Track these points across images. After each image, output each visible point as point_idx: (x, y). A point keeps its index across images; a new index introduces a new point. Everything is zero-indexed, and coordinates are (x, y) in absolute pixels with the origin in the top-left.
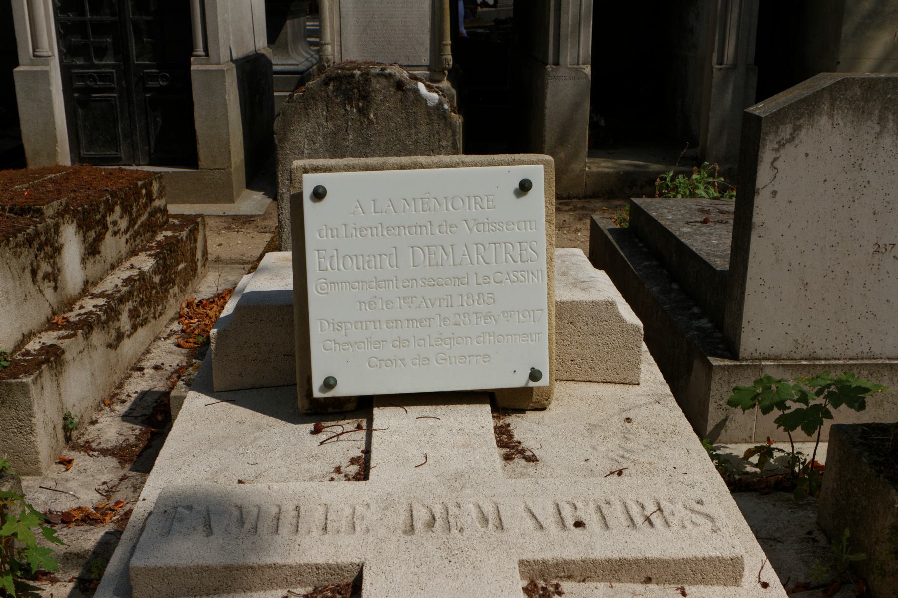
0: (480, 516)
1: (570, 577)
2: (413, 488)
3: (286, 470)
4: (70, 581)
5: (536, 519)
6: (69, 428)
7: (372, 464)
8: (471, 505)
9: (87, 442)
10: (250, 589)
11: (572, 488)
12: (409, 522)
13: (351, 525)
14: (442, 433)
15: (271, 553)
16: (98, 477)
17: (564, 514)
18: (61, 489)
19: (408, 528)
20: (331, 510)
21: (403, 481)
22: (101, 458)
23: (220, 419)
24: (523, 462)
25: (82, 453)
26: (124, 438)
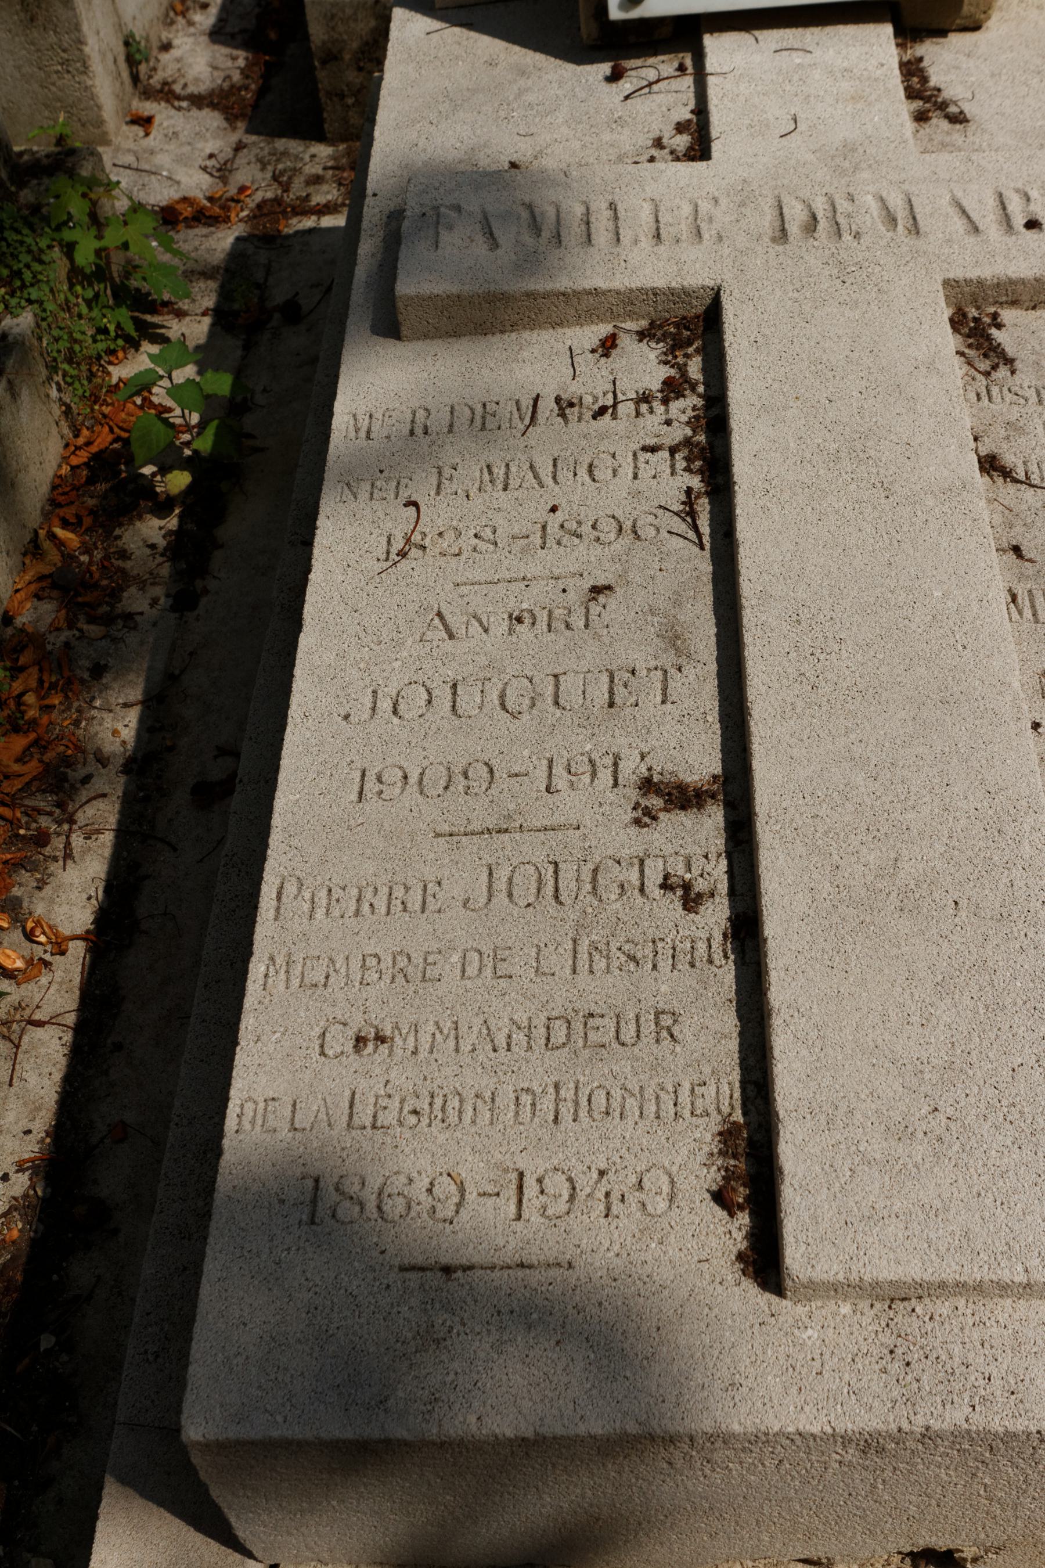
0: (884, 213)
1: (1014, 303)
2: (781, 171)
3: (577, 145)
4: (204, 314)
5: (968, 217)
6: (134, 56)
7: (714, 133)
8: (870, 197)
9: (165, 83)
10: (561, 324)
11: (1024, 168)
12: (778, 223)
13: (694, 231)
14: (817, 77)
15: (588, 273)
16: (200, 145)
17: (1010, 208)
18: (147, 167)
19: (778, 234)
20: (662, 208)
21: (765, 160)
22: (195, 112)
23: (457, 58)
24: (945, 124)
25: (163, 104)
26: (222, 74)
